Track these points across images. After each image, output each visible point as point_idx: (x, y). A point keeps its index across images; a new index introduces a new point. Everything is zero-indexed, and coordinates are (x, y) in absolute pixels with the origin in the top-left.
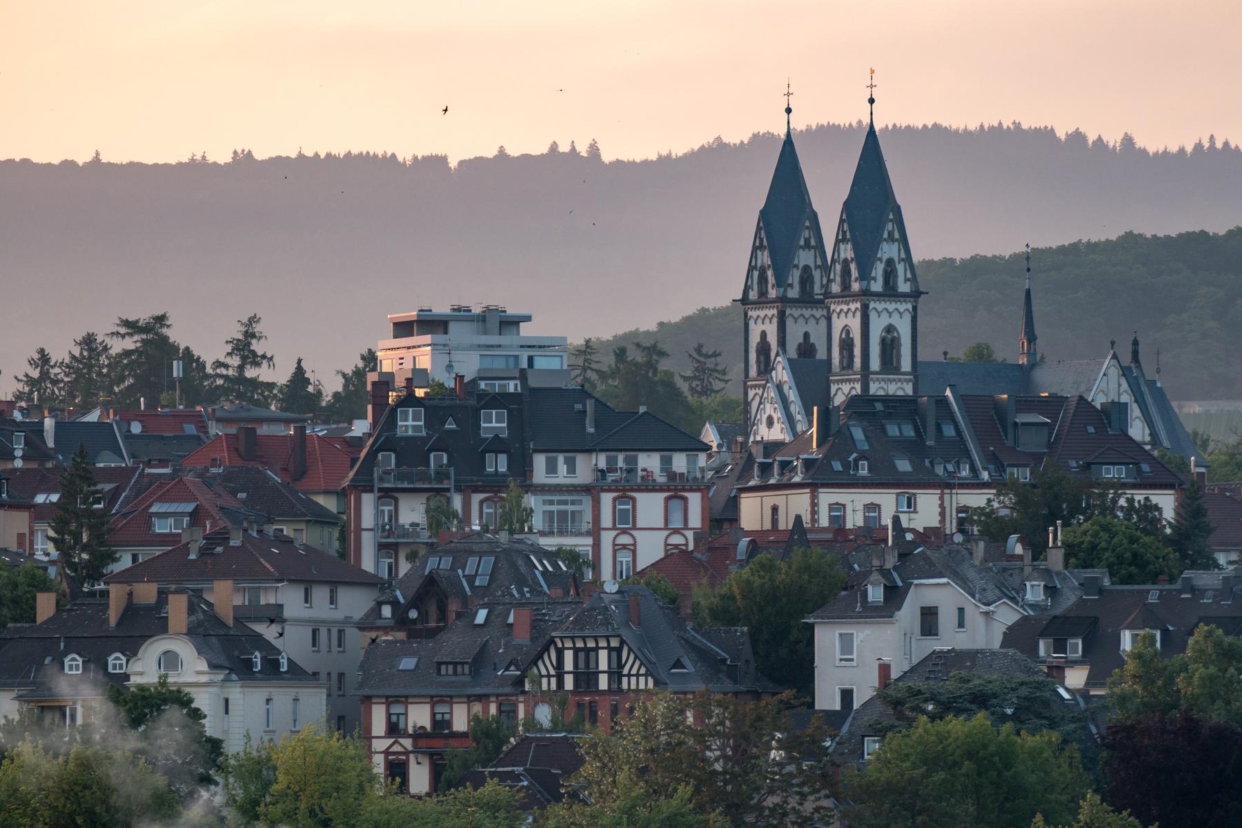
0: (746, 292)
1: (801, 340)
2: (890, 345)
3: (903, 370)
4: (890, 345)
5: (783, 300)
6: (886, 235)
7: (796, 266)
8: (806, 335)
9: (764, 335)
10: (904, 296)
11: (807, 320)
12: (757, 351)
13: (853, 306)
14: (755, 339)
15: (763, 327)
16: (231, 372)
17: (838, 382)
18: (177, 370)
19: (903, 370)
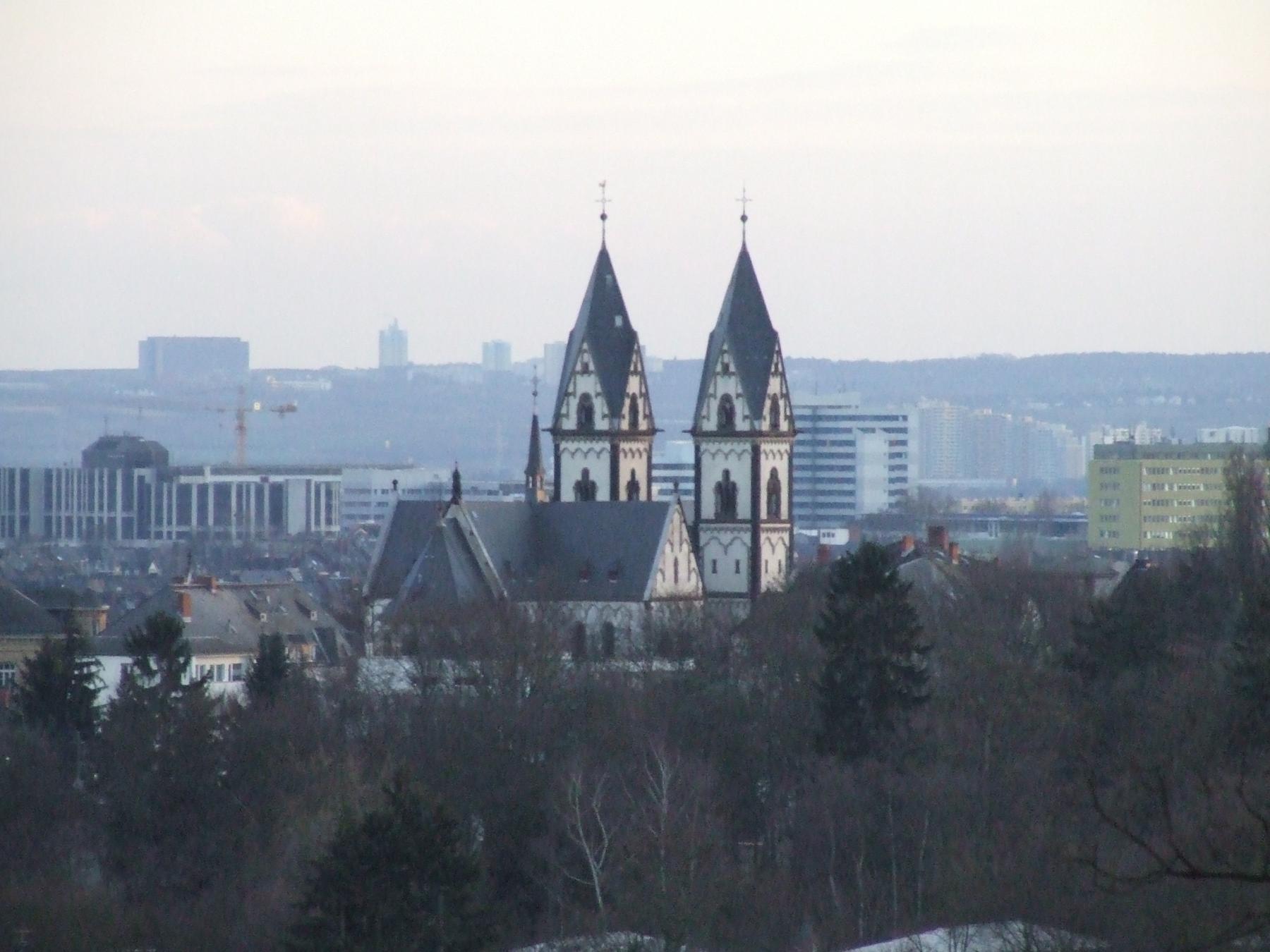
0: (698, 417)
1: (579, 478)
2: (726, 491)
3: (740, 517)
4: (726, 491)
5: (754, 434)
6: (632, 368)
7: (714, 396)
8: (586, 473)
9: (774, 473)
10: (601, 435)
11: (726, 456)
12: (768, 489)
13: (598, 446)
14: (624, 479)
15: (584, 464)
16: (313, 528)
17: (768, 530)
18: (182, 660)
19: (740, 517)
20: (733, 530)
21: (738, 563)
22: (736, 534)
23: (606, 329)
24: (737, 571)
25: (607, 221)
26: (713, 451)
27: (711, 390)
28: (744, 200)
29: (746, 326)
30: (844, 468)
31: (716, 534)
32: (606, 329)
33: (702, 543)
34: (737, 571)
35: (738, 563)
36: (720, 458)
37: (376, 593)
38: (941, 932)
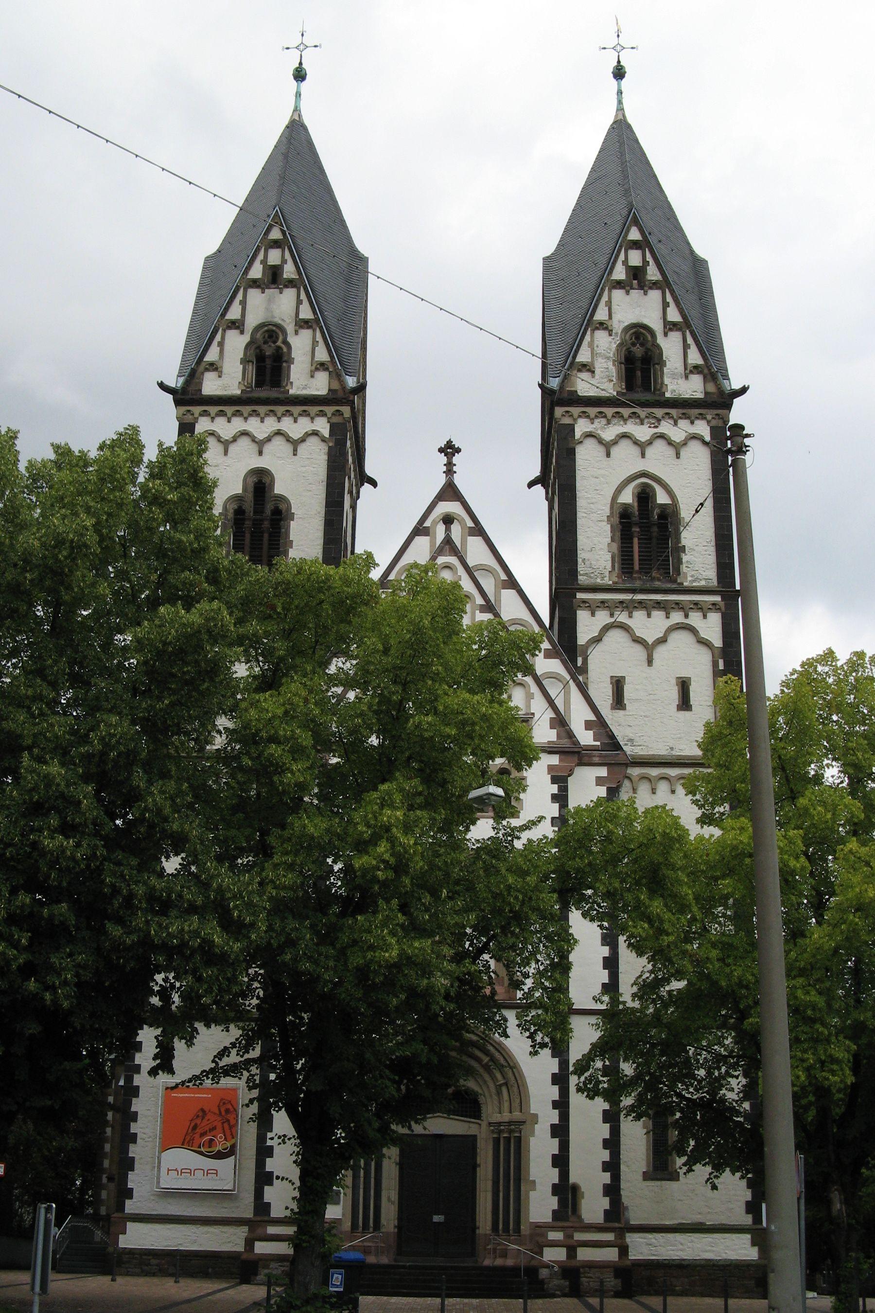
13: (296, 428)
20: (665, 607)
21: (684, 686)
22: (677, 617)
23: (293, 242)
24: (685, 704)
25: (304, 85)
26: (609, 434)
27: (601, 315)
28: (618, 48)
29: (625, 239)
30: (645, 560)
31: (622, 617)
32: (293, 242)
33: (582, 638)
34: (685, 704)
35: (684, 686)
36: (624, 452)
37: (159, 840)
38: (256, 1111)
